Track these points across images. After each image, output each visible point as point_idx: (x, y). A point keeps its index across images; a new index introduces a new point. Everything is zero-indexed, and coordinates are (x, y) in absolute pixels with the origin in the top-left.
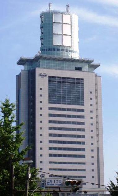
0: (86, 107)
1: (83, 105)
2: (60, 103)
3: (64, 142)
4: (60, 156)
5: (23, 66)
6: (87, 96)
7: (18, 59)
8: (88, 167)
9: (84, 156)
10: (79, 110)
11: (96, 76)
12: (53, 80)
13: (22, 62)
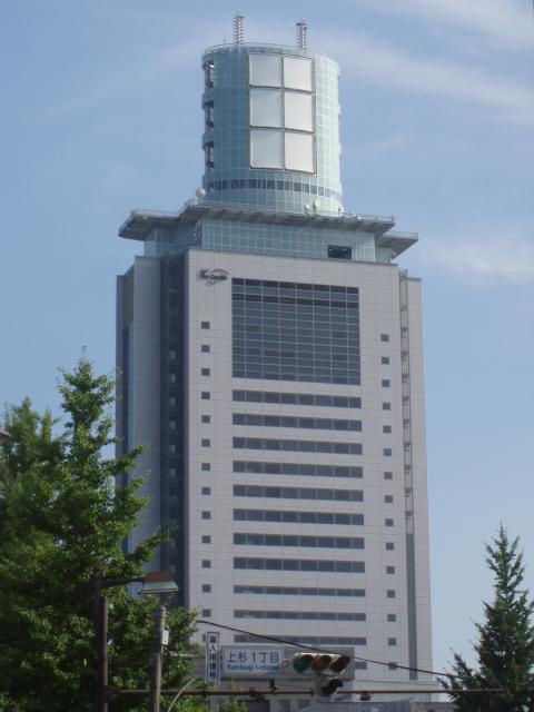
0: (368, 389)
1: (357, 382)
2: (275, 377)
3: (290, 517)
7: (123, 219)
8: (374, 606)
9: (359, 567)
10: (340, 402)
12: (247, 293)
13: (136, 228)
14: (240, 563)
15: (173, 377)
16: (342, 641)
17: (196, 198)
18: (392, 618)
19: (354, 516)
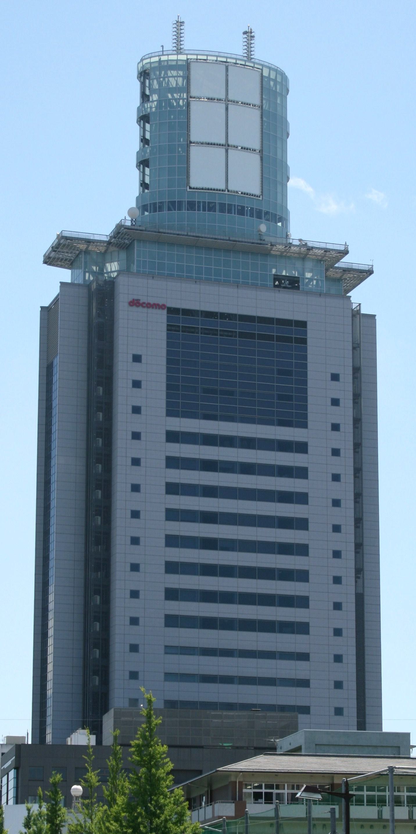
0: (316, 433)
1: (304, 425)
2: (213, 418)
3: (227, 571)
7: (48, 241)
8: (320, 671)
10: (285, 446)
11: (356, 314)
12: (182, 323)
16: (283, 708)
17: (129, 218)
18: (337, 606)
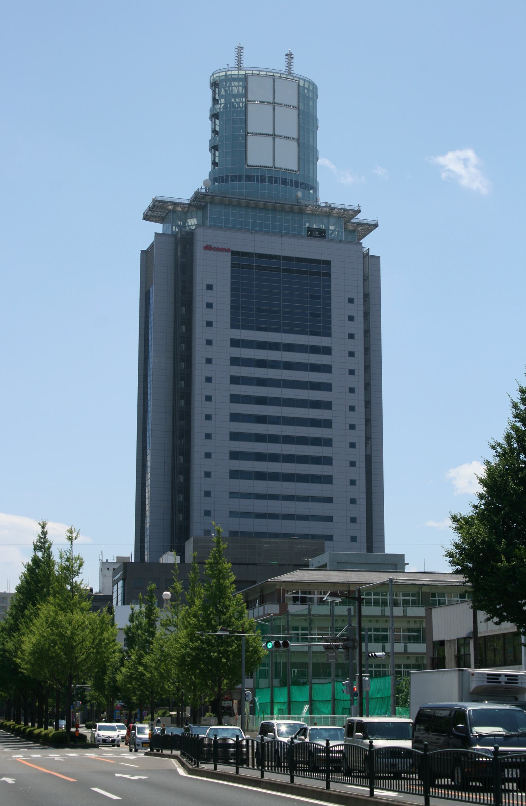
0: (337, 341)
1: (329, 335)
3: (274, 439)
4: (261, 476)
5: (162, 225)
6: (339, 310)
7: (147, 203)
9: (328, 480)
13: (158, 211)
14: (234, 474)
15: (181, 478)
16: (314, 537)
19: (325, 384)
